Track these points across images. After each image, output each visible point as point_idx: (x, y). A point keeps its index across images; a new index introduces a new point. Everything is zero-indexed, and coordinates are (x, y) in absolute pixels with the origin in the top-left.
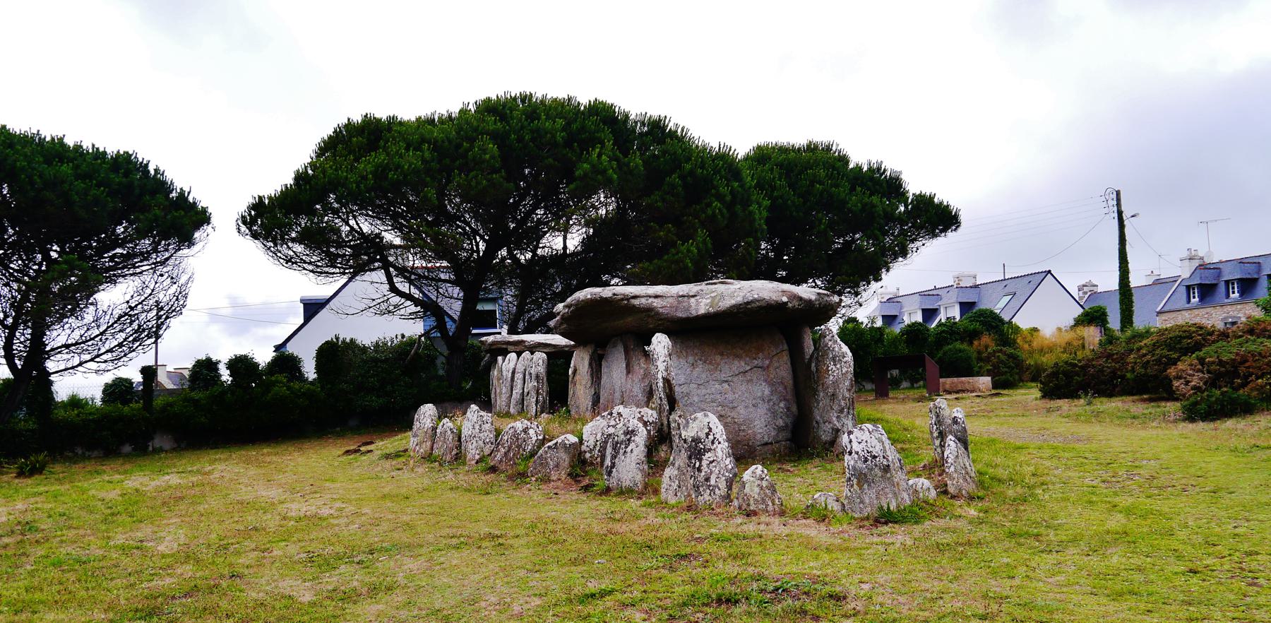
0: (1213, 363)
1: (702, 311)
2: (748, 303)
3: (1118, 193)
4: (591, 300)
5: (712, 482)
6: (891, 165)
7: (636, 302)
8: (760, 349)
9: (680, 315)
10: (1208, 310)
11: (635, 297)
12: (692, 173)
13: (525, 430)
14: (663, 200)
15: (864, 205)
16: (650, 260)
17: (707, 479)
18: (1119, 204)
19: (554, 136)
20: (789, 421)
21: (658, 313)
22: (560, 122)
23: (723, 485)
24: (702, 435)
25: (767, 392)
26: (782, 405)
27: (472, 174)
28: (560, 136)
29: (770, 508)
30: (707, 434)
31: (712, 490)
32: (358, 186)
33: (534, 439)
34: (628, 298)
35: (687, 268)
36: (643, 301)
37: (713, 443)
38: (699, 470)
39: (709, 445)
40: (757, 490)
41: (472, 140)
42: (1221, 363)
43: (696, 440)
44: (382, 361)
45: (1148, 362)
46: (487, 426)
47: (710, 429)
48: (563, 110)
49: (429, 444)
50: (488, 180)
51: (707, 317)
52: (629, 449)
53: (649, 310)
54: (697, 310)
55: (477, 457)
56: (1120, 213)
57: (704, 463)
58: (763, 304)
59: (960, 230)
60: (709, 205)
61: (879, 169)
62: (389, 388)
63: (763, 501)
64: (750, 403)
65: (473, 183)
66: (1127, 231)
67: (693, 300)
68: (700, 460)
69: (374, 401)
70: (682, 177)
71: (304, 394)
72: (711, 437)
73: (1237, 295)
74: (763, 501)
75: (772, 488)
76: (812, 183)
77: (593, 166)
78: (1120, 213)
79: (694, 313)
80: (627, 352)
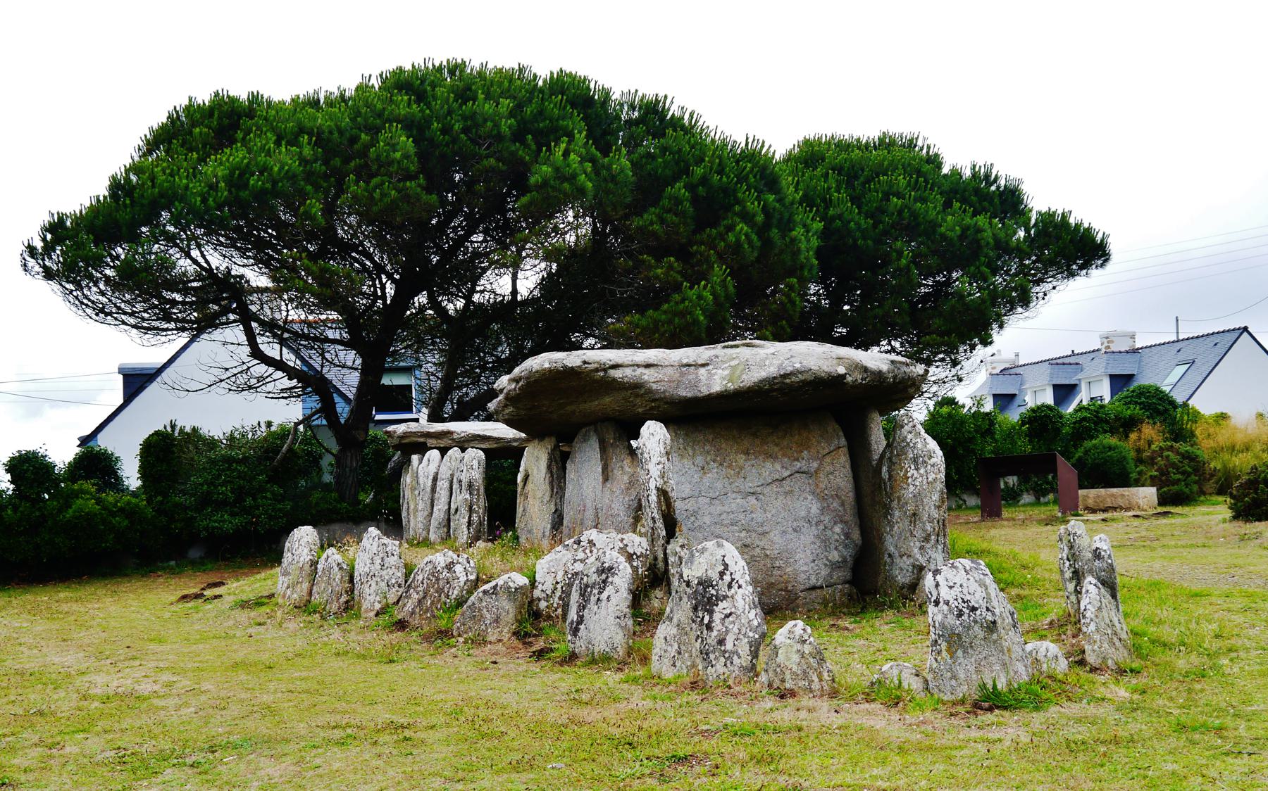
1: (716, 388)
2: (786, 376)
4: (550, 370)
6: (1006, 169)
8: (805, 446)
11: (616, 366)
13: (450, 567)
14: (662, 221)
15: (965, 229)
17: (721, 642)
19: (497, 125)
20: (848, 553)
21: (650, 391)
22: (506, 104)
23: (744, 650)
24: (714, 576)
25: (815, 509)
26: (837, 529)
27: (375, 181)
28: (506, 125)
30: (722, 574)
35: (696, 321)
36: (628, 372)
37: (730, 586)
39: (724, 590)
41: (375, 131)
43: (705, 583)
44: (239, 462)
46: (393, 560)
47: (726, 566)
48: (512, 86)
49: (306, 586)
50: (399, 191)
51: (724, 398)
52: (604, 596)
54: (709, 386)
55: (377, 606)
60: (731, 228)
62: (249, 501)
67: (702, 371)
68: (711, 612)
69: (227, 522)
70: (690, 187)
71: (122, 510)
72: (727, 578)
76: (886, 197)
77: (557, 169)
79: (705, 391)
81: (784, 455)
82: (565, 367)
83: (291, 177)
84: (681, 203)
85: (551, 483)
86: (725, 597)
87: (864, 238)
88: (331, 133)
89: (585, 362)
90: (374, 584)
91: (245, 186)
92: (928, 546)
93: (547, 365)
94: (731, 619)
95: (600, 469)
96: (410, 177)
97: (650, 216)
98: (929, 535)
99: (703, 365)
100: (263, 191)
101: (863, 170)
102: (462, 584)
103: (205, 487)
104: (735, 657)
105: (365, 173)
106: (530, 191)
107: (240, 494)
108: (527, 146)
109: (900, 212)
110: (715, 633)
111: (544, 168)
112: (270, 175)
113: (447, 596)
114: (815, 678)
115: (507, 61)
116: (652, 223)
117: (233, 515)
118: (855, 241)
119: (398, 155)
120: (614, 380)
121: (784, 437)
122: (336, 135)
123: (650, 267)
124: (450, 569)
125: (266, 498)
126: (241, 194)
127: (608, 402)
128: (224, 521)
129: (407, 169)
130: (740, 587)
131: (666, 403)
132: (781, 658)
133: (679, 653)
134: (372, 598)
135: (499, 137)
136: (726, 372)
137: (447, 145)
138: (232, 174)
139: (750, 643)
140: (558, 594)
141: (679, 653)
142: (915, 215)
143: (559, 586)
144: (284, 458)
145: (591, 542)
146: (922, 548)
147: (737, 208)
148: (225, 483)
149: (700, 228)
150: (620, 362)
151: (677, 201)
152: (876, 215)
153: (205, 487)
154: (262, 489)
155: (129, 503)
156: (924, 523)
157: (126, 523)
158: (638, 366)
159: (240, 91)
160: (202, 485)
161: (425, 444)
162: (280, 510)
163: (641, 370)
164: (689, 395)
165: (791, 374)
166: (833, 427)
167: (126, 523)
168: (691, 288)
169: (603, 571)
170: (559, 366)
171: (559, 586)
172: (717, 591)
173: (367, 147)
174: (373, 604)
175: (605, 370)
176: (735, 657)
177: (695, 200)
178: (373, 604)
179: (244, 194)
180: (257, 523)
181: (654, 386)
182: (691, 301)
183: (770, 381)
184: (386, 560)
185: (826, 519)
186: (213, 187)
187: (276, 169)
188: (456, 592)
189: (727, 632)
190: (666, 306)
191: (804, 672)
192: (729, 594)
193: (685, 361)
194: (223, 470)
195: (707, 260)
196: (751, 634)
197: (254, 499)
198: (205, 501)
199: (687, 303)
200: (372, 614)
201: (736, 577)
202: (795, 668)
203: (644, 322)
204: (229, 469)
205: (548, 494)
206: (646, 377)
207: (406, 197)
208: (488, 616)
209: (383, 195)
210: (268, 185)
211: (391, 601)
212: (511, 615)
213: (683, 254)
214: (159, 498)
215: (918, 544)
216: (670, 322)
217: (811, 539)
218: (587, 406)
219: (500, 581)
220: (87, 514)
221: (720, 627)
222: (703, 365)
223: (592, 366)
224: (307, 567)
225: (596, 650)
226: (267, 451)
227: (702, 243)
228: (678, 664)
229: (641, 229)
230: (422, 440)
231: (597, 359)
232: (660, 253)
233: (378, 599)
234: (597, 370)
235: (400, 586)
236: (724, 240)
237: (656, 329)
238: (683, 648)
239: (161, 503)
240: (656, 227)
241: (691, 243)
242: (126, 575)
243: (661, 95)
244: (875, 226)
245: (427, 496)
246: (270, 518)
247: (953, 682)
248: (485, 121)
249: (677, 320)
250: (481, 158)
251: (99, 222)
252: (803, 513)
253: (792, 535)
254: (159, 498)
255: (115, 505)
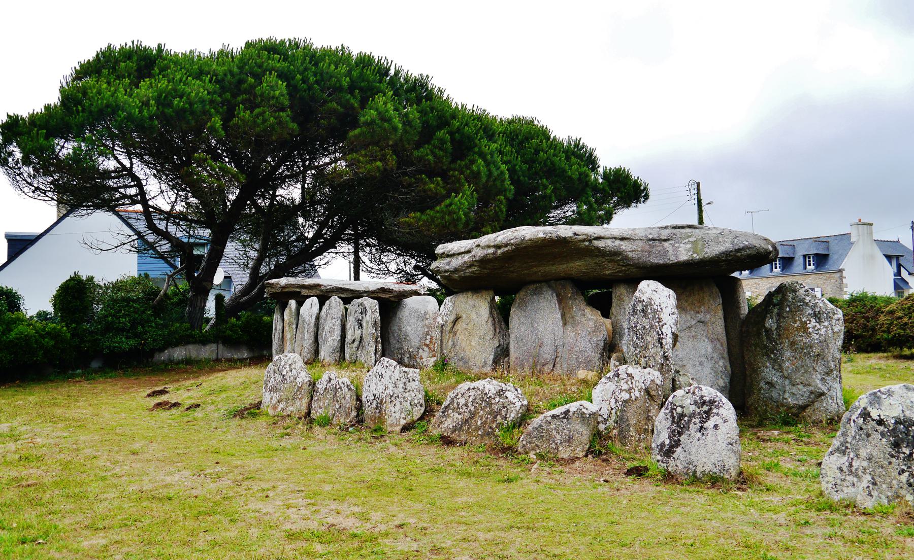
1: (684, 257)
2: (738, 250)
3: (698, 184)
4: (544, 240)
6: (589, 142)
7: (600, 244)
8: (701, 303)
10: (756, 280)
11: (599, 238)
13: (500, 393)
14: (433, 153)
15: (580, 174)
16: (422, 211)
18: (698, 193)
19: (339, 80)
22: (343, 69)
25: (710, 350)
26: (721, 363)
27: (257, 111)
28: (345, 82)
32: (140, 112)
33: (518, 404)
36: (609, 243)
41: (258, 78)
44: (134, 301)
45: (906, 324)
46: (414, 385)
48: (339, 57)
49: (305, 401)
50: (276, 118)
52: (710, 424)
53: (615, 254)
54: (676, 256)
55: (403, 422)
56: (699, 201)
58: (753, 252)
59: (648, 202)
60: (473, 162)
61: (577, 145)
62: (140, 328)
65: (259, 121)
66: (704, 214)
67: (666, 244)
69: (126, 343)
70: (451, 133)
71: (48, 333)
76: (537, 152)
78: (699, 201)
79: (673, 259)
81: (691, 309)
83: (203, 101)
84: (445, 143)
85: (494, 324)
87: (524, 176)
88: (225, 75)
89: (575, 234)
90: (398, 404)
91: (170, 105)
92: (828, 378)
95: (559, 316)
96: (283, 109)
97: (425, 151)
98: (832, 371)
99: (665, 240)
100: (183, 110)
101: (517, 136)
102: (518, 408)
103: (110, 318)
105: (251, 106)
106: (360, 127)
107: (134, 323)
108: (355, 97)
109: (545, 162)
111: (372, 112)
112: (188, 99)
113: (505, 419)
116: (427, 155)
117: (127, 338)
118: (519, 177)
119: (277, 93)
120: (598, 248)
121: (689, 296)
122: (229, 76)
123: (425, 184)
125: (151, 326)
126: (166, 110)
127: (577, 266)
128: (123, 342)
129: (282, 104)
131: (637, 267)
134: (397, 415)
135: (341, 89)
136: (689, 246)
137: (305, 91)
138: (160, 96)
140: (613, 417)
142: (553, 163)
143: (613, 412)
144: (161, 300)
147: (476, 149)
148: (124, 316)
149: (453, 161)
150: (602, 235)
151: (442, 141)
152: (531, 162)
153: (110, 318)
154: (148, 321)
155: (54, 328)
156: (828, 362)
157: (52, 343)
158: (615, 238)
159: (151, 43)
160: (107, 316)
161: (300, 292)
162: (160, 335)
163: (617, 242)
164: (661, 262)
165: (743, 249)
166: (715, 290)
167: (52, 343)
170: (554, 236)
171: (613, 412)
173: (253, 87)
174: (398, 420)
175: (590, 241)
177: (453, 140)
178: (398, 420)
179: (169, 111)
180: (144, 344)
181: (630, 255)
183: (726, 253)
184: (408, 384)
185: (715, 355)
186: (146, 104)
187: (193, 95)
188: (512, 415)
190: (438, 208)
193: (651, 237)
194: (123, 307)
195: (459, 180)
197: (143, 327)
198: (109, 328)
199: (453, 206)
200: (398, 428)
203: (424, 217)
204: (127, 306)
206: (624, 248)
207: (280, 122)
208: (558, 436)
209: (264, 121)
210: (187, 106)
211: (415, 418)
213: (444, 175)
214: (74, 325)
215: (819, 377)
216: (443, 218)
217: (709, 371)
218: (547, 269)
220: (26, 336)
222: (665, 240)
223: (581, 237)
224: (306, 386)
226: (149, 294)
227: (455, 170)
228: (875, 493)
229: (420, 159)
230: (298, 290)
231: (586, 232)
232: (431, 175)
233: (403, 415)
234: (584, 240)
235: (421, 406)
236: (469, 169)
237: (433, 221)
239: (75, 328)
240: (430, 157)
241: (450, 169)
242: (51, 381)
244: (529, 169)
245: (312, 329)
246: (154, 340)
248: (331, 77)
250: (325, 102)
251: (53, 123)
252: (703, 352)
253: (699, 368)
254: (74, 325)
255: (44, 330)
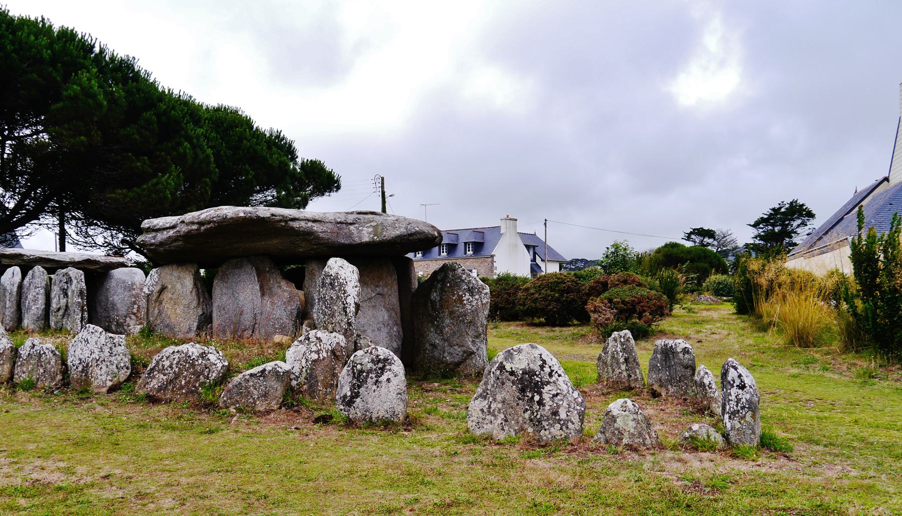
0: (618, 303)
1: (366, 239)
2: (411, 235)
3: (383, 179)
5: (563, 415)
7: (295, 225)
9: (342, 241)
12: (165, 112)
15: (280, 162)
17: (555, 413)
18: (383, 187)
20: (400, 343)
21: (318, 238)
23: (575, 418)
24: (537, 368)
25: (386, 317)
26: (395, 329)
28: (47, 54)
29: (648, 442)
30: (542, 367)
31: (564, 424)
34: (286, 220)
35: (166, 198)
36: (303, 224)
37: (550, 375)
38: (541, 403)
39: (546, 378)
40: (632, 424)
42: (623, 302)
43: (529, 373)
45: (537, 299)
46: (121, 349)
47: (544, 362)
51: (370, 245)
52: (384, 378)
53: (308, 235)
54: (360, 238)
55: (109, 384)
57: (546, 397)
58: (422, 237)
60: (180, 144)
63: (640, 434)
64: (375, 327)
67: (352, 227)
68: (540, 394)
70: (158, 115)
72: (547, 370)
73: (471, 252)
74: (640, 434)
75: (648, 421)
77: (83, 89)
79: (357, 240)
80: (260, 274)
82: (258, 217)
85: (198, 295)
86: (548, 383)
89: (273, 215)
90: (104, 367)
93: (242, 215)
94: (559, 397)
95: (258, 287)
99: (351, 224)
102: (219, 369)
104: (570, 424)
110: (547, 408)
113: (208, 378)
114: (647, 437)
115: (33, 14)
120: (293, 228)
124: (203, 358)
127: (275, 243)
130: (559, 376)
132: (619, 423)
133: (506, 421)
136: (371, 230)
139: (578, 413)
140: (304, 375)
141: (506, 421)
145: (319, 339)
146: (473, 342)
147: (183, 132)
150: (297, 217)
156: (477, 327)
158: (309, 220)
163: (310, 224)
168: (163, 176)
169: (379, 361)
171: (304, 370)
172: (541, 378)
175: (286, 222)
176: (570, 424)
181: (321, 235)
182: (163, 184)
184: (114, 349)
188: (214, 375)
189: (558, 406)
191: (640, 433)
192: (551, 380)
196: (578, 408)
199: (160, 186)
200: (104, 390)
201: (555, 368)
202: (632, 431)
205: (195, 303)
206: (315, 228)
208: (255, 392)
212: (279, 392)
219: (269, 366)
221: (551, 403)
222: (351, 224)
225: (374, 416)
228: (506, 428)
231: (282, 214)
233: (109, 378)
234: (280, 221)
235: (127, 368)
238: (509, 417)
240: (137, 137)
243: (131, 56)
247: (753, 436)
249: (154, 196)
252: (381, 319)
253: (377, 333)
